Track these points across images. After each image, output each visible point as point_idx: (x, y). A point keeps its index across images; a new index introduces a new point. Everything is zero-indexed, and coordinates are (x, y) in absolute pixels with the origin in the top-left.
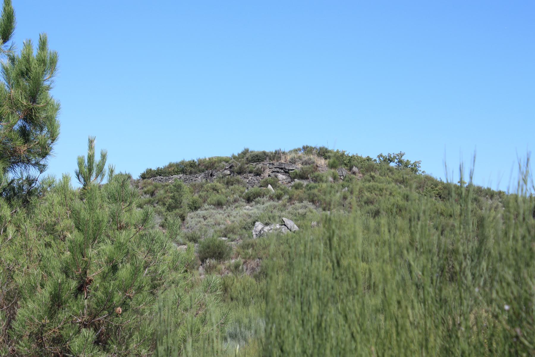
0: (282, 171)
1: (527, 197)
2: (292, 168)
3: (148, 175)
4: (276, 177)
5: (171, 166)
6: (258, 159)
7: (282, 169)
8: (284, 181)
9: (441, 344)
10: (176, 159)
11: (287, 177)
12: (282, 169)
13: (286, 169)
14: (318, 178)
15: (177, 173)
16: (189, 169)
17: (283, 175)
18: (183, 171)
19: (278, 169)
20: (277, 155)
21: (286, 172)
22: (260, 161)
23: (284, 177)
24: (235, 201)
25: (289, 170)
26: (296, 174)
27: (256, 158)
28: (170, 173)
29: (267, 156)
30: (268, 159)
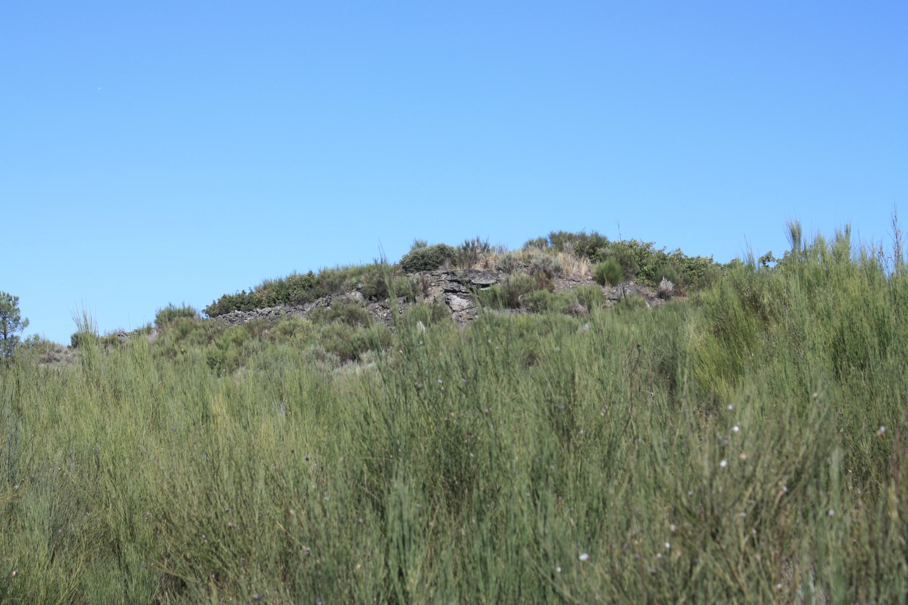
2: (484, 282)
4: (447, 303)
6: (426, 264)
8: (463, 312)
15: (272, 302)
18: (287, 299)
19: (455, 284)
23: (465, 303)
27: (422, 261)
28: (259, 304)
29: (449, 255)
30: (447, 264)
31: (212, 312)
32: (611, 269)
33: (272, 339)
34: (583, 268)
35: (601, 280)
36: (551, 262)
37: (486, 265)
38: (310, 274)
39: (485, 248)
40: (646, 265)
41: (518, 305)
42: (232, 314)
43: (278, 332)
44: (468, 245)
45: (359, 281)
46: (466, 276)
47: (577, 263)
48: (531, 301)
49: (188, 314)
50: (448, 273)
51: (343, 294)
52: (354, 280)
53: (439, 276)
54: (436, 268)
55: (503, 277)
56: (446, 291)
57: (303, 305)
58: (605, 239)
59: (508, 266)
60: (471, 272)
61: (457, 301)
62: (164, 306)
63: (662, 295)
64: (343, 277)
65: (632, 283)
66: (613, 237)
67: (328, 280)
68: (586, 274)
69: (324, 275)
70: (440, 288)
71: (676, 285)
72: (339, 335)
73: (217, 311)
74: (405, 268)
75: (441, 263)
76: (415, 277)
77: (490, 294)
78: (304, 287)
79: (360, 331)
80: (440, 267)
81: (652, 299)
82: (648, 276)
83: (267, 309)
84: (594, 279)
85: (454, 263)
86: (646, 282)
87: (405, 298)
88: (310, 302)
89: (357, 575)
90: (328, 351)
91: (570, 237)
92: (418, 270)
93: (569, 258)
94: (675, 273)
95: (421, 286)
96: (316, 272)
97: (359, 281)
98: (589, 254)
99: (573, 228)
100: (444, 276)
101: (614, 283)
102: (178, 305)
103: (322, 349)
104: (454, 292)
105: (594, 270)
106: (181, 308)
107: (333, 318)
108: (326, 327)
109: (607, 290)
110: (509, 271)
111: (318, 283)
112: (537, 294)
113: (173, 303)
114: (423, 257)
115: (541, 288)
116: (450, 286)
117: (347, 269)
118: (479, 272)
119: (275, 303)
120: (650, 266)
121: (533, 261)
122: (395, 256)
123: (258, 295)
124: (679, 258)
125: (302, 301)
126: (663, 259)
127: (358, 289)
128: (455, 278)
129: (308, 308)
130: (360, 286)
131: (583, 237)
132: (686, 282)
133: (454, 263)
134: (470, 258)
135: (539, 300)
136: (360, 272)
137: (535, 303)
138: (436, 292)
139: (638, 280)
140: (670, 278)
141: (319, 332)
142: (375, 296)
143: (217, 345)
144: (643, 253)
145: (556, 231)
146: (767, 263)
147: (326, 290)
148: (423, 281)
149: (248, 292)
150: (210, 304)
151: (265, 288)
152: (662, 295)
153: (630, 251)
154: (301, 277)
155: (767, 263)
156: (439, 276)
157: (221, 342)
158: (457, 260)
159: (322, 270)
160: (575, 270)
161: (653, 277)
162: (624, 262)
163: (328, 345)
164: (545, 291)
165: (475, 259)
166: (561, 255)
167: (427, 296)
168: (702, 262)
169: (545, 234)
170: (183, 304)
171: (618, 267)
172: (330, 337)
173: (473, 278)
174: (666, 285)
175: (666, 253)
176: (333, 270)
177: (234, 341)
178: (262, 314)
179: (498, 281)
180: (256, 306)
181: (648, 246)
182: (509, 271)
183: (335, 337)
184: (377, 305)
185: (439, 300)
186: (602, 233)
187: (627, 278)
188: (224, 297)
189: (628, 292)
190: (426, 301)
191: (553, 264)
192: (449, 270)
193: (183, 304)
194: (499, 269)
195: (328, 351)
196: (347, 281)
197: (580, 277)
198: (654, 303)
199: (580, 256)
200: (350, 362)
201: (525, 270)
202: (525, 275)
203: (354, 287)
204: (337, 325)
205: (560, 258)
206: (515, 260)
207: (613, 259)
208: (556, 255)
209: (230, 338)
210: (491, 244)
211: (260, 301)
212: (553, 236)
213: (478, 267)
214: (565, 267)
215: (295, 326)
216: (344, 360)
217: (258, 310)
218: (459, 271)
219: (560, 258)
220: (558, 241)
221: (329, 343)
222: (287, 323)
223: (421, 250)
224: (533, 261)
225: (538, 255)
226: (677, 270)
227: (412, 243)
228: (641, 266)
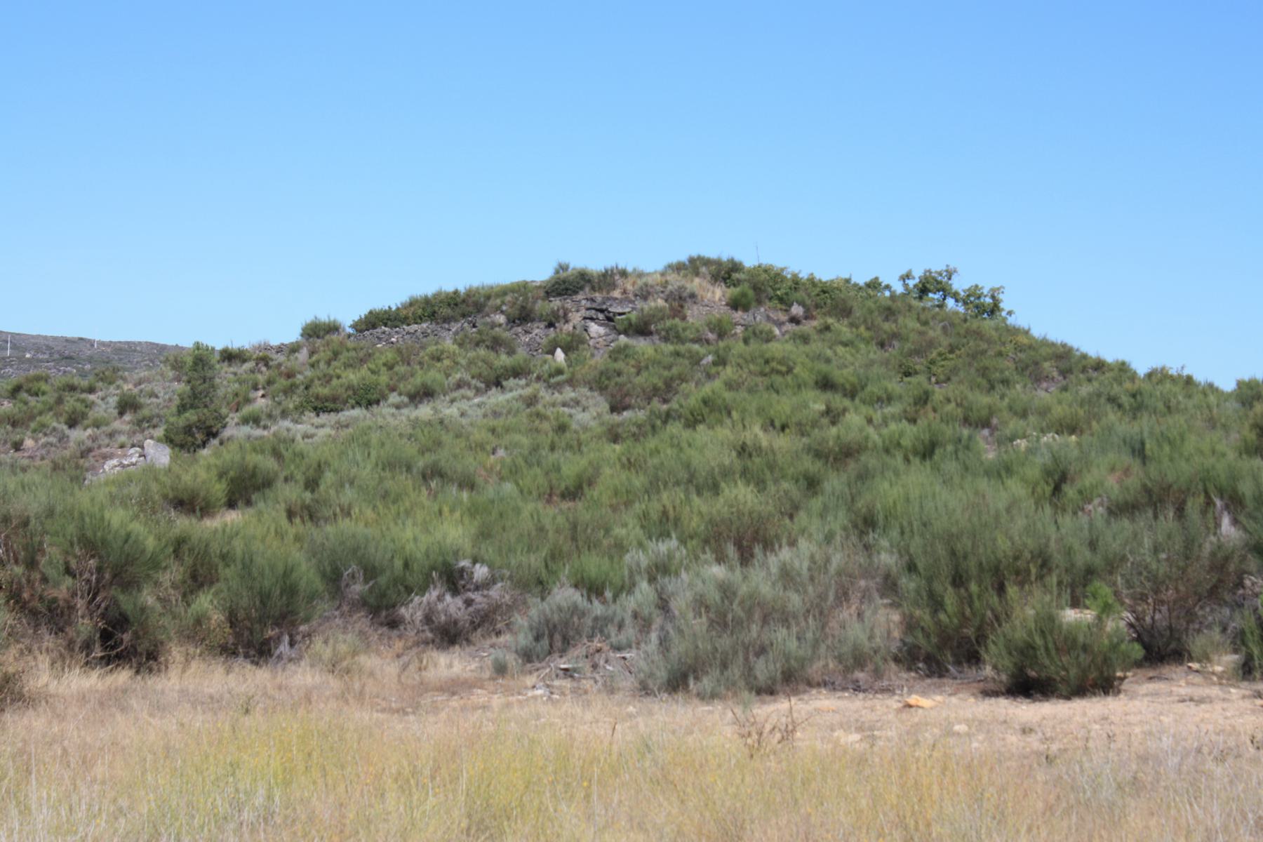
0: (601, 316)
1: (1160, 575)
2: (620, 310)
3: (373, 321)
4: (586, 330)
5: (412, 303)
6: (567, 289)
7: (602, 311)
8: (600, 339)
9: (1108, 617)
10: (426, 286)
11: (608, 330)
12: (602, 311)
13: (609, 312)
14: (672, 334)
15: (419, 319)
16: (446, 311)
17: (601, 325)
18: (433, 316)
19: (593, 312)
20: (607, 280)
21: (609, 319)
22: (569, 292)
23: (602, 330)
24: (459, 385)
25: (615, 314)
26: (630, 324)
27: (563, 287)
28: (406, 320)
29: (589, 281)
30: (587, 289)
31: (358, 328)
32: (744, 295)
33: (421, 363)
34: (718, 293)
35: (735, 305)
36: (686, 289)
37: (625, 292)
38: (456, 292)
39: (624, 274)
40: (779, 289)
41: (650, 333)
42: (378, 330)
43: (426, 358)
44: (607, 271)
45: (503, 303)
46: (604, 303)
47: (711, 288)
48: (663, 329)
49: (333, 328)
50: (587, 299)
51: (488, 315)
52: (498, 301)
53: (580, 301)
54: (576, 293)
55: (639, 304)
56: (585, 318)
57: (449, 323)
58: (741, 264)
59: (645, 294)
60: (608, 299)
61: (595, 328)
62: (309, 318)
63: (794, 320)
64: (488, 297)
65: (762, 310)
66: (749, 262)
67: (474, 299)
68: (720, 300)
69: (470, 293)
70: (579, 314)
71: (807, 310)
72: (483, 361)
73: (364, 327)
74: (547, 293)
75: (582, 288)
76: (556, 303)
77: (625, 322)
78: (449, 305)
79: (504, 360)
80: (581, 292)
81: (783, 323)
82: (781, 300)
83: (415, 327)
84: (727, 305)
85: (593, 289)
86: (779, 306)
87: (546, 323)
88: (456, 321)
89: (410, 563)
90: (473, 377)
91: (707, 262)
92: (559, 294)
93: (705, 284)
94: (806, 298)
95: (561, 313)
96: (462, 289)
97: (503, 303)
98: (725, 280)
99: (711, 253)
100: (584, 302)
101: (746, 309)
102: (324, 317)
103: (467, 377)
104: (592, 319)
105: (728, 295)
106: (327, 320)
107: (477, 345)
108: (471, 354)
109: (738, 316)
110: (645, 298)
111: (464, 301)
112: (669, 323)
113: (319, 317)
114: (564, 282)
115: (673, 318)
116: (588, 314)
117: (492, 288)
118: (616, 299)
119: (421, 319)
120: (783, 291)
121: (670, 287)
122: (541, 273)
123: (405, 312)
124: (812, 282)
125: (447, 320)
126: (796, 283)
127: (502, 312)
128: (594, 305)
129: (455, 327)
130: (504, 308)
131: (718, 263)
132: (817, 306)
133: (593, 289)
134: (609, 285)
135: (671, 329)
136: (504, 291)
137: (667, 331)
138: (576, 318)
139: (771, 304)
140: (801, 303)
141: (464, 358)
142: (519, 319)
143: (369, 369)
144: (775, 277)
145: (694, 254)
146: (907, 281)
147: (471, 309)
148: (563, 308)
149: (394, 308)
150: (357, 318)
151: (411, 304)
152: (794, 320)
153: (764, 276)
154: (447, 294)
155: (907, 281)
156: (580, 301)
157: (372, 366)
158: (596, 286)
159: (468, 287)
160: (709, 295)
161: (785, 302)
162: (757, 288)
163: (473, 371)
164: (677, 320)
165: (613, 286)
166: (697, 280)
167: (567, 321)
168: (835, 285)
169: (683, 257)
170: (329, 317)
171: (751, 293)
172: (475, 364)
173: (611, 305)
174: (797, 310)
175: (801, 276)
176: (478, 288)
177: (384, 365)
178: (408, 333)
179: (633, 309)
180: (403, 323)
181: (782, 270)
182: (645, 298)
183: (480, 364)
184: (519, 329)
185: (578, 327)
186: (738, 257)
187: (759, 302)
188: (371, 312)
189: (758, 318)
190: (566, 327)
191: (688, 291)
192: (589, 296)
193: (329, 317)
194: (636, 295)
195: (473, 377)
196: (491, 303)
197: (714, 302)
198: (784, 328)
199: (716, 280)
200: (494, 389)
201: (662, 295)
202: (661, 302)
203: (498, 309)
204: (482, 352)
205: (695, 284)
206: (652, 287)
207: (746, 285)
208: (692, 281)
209: (381, 362)
210: (630, 269)
211: (406, 318)
212: (692, 261)
213: (616, 294)
214: (699, 292)
215: (442, 352)
216: (488, 387)
217: (405, 327)
218: (598, 296)
219: (695, 284)
220: (694, 266)
221: (475, 370)
222: (435, 348)
223: (563, 275)
224: (670, 287)
225: (675, 281)
226: (809, 295)
227: (555, 265)
228: (775, 290)
